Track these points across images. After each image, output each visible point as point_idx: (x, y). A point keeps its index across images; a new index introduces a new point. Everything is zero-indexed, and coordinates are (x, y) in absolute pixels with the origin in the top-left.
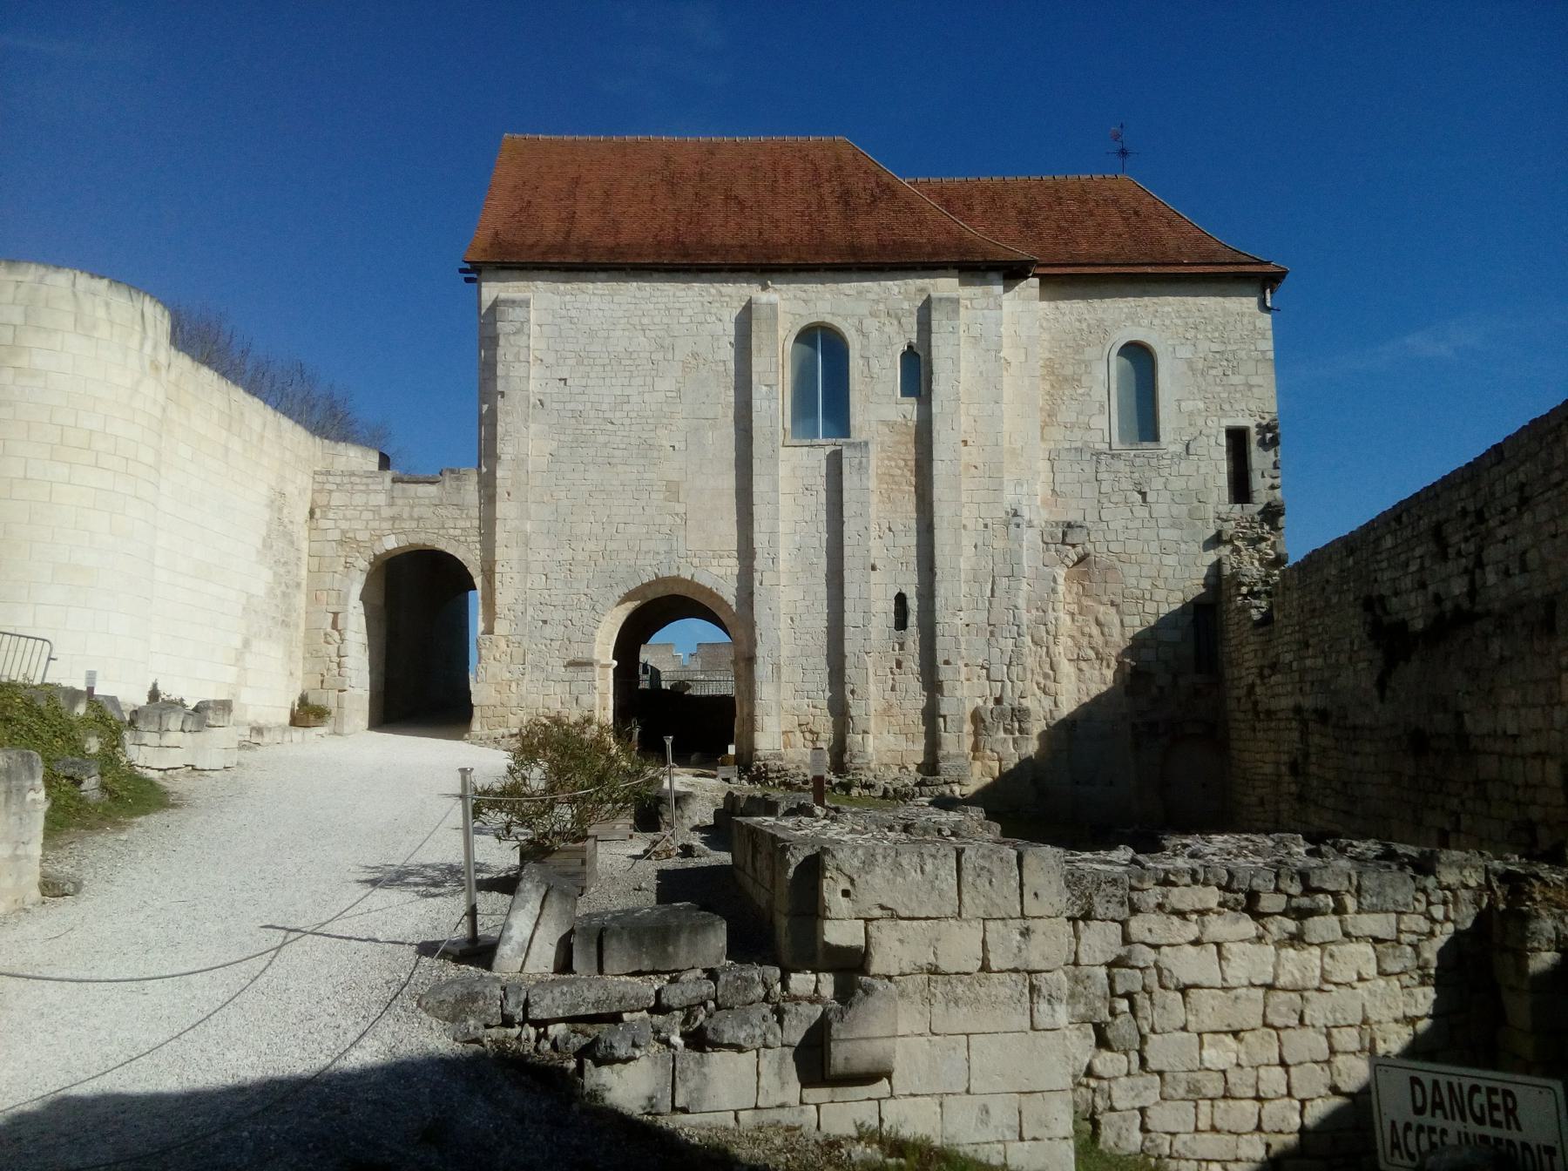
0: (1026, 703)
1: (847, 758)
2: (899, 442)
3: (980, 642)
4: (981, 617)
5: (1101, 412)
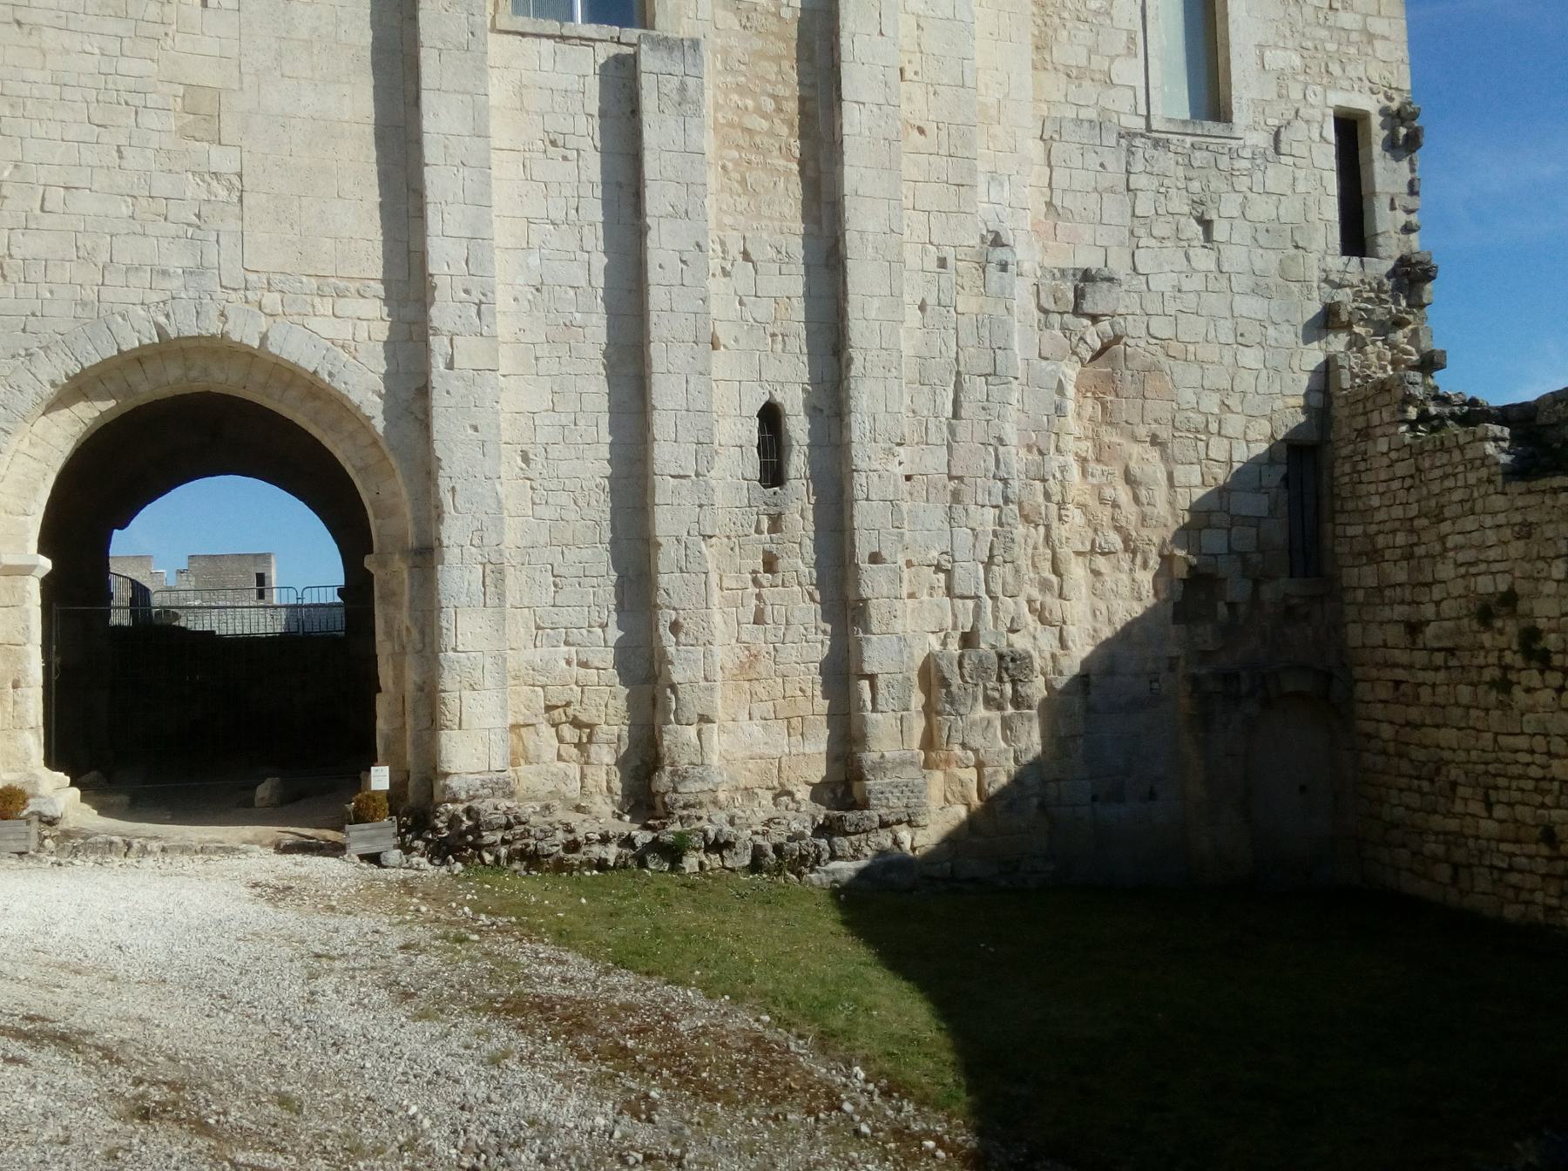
0: (1020, 642)
1: (663, 781)
2: (761, 55)
4: (936, 461)
5: (1131, 53)
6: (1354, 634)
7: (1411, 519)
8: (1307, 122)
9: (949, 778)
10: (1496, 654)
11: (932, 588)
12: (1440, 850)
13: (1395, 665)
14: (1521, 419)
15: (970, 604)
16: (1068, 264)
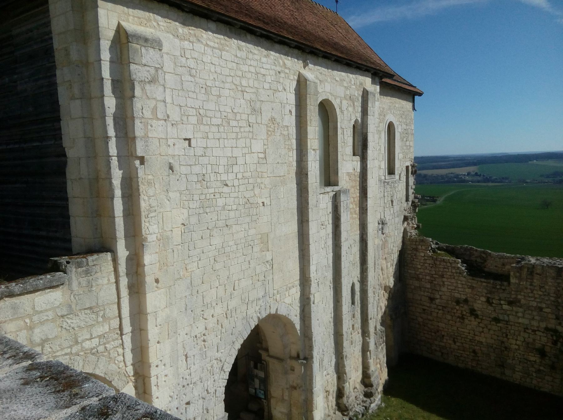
1: (345, 399)
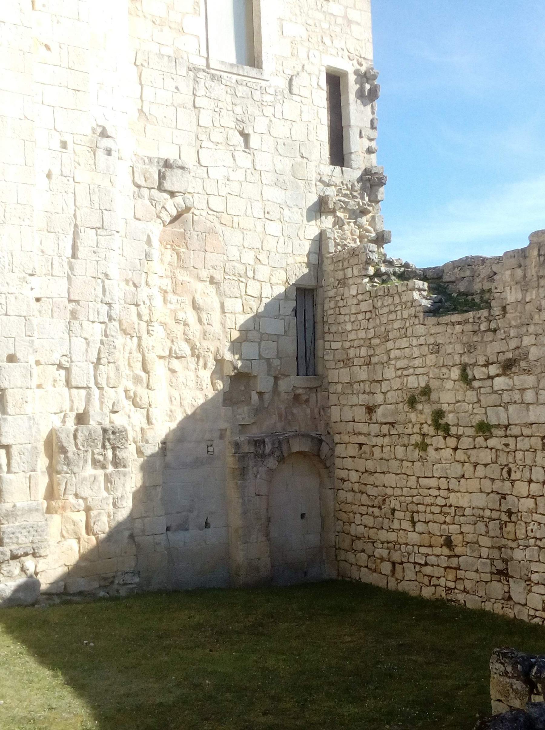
0: (119, 421)
3: (58, 326)
4: (58, 288)
6: (335, 413)
7: (370, 339)
8: (310, 74)
9: (65, 520)
10: (419, 426)
11: (55, 381)
12: (385, 553)
13: (360, 434)
14: (436, 279)
15: (83, 392)
16: (154, 154)
